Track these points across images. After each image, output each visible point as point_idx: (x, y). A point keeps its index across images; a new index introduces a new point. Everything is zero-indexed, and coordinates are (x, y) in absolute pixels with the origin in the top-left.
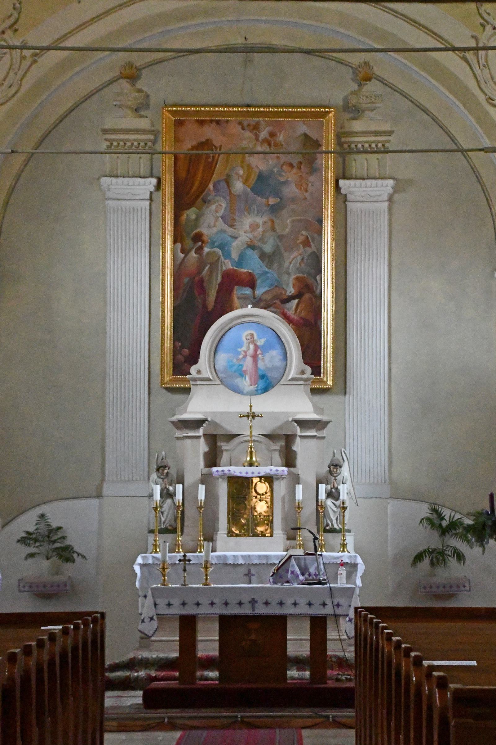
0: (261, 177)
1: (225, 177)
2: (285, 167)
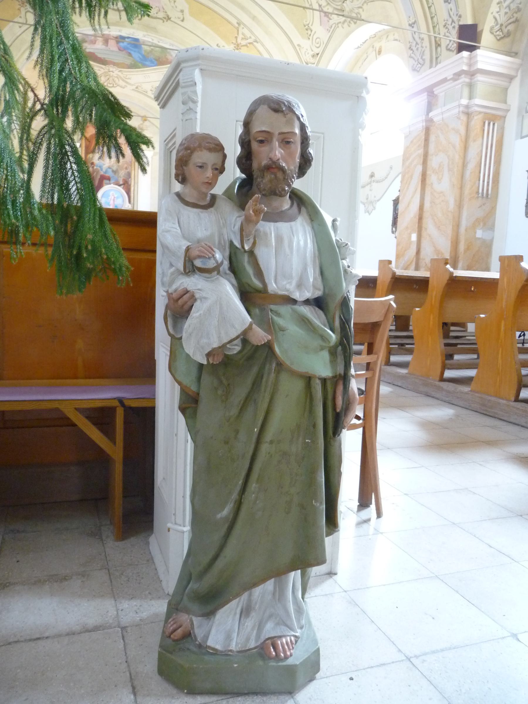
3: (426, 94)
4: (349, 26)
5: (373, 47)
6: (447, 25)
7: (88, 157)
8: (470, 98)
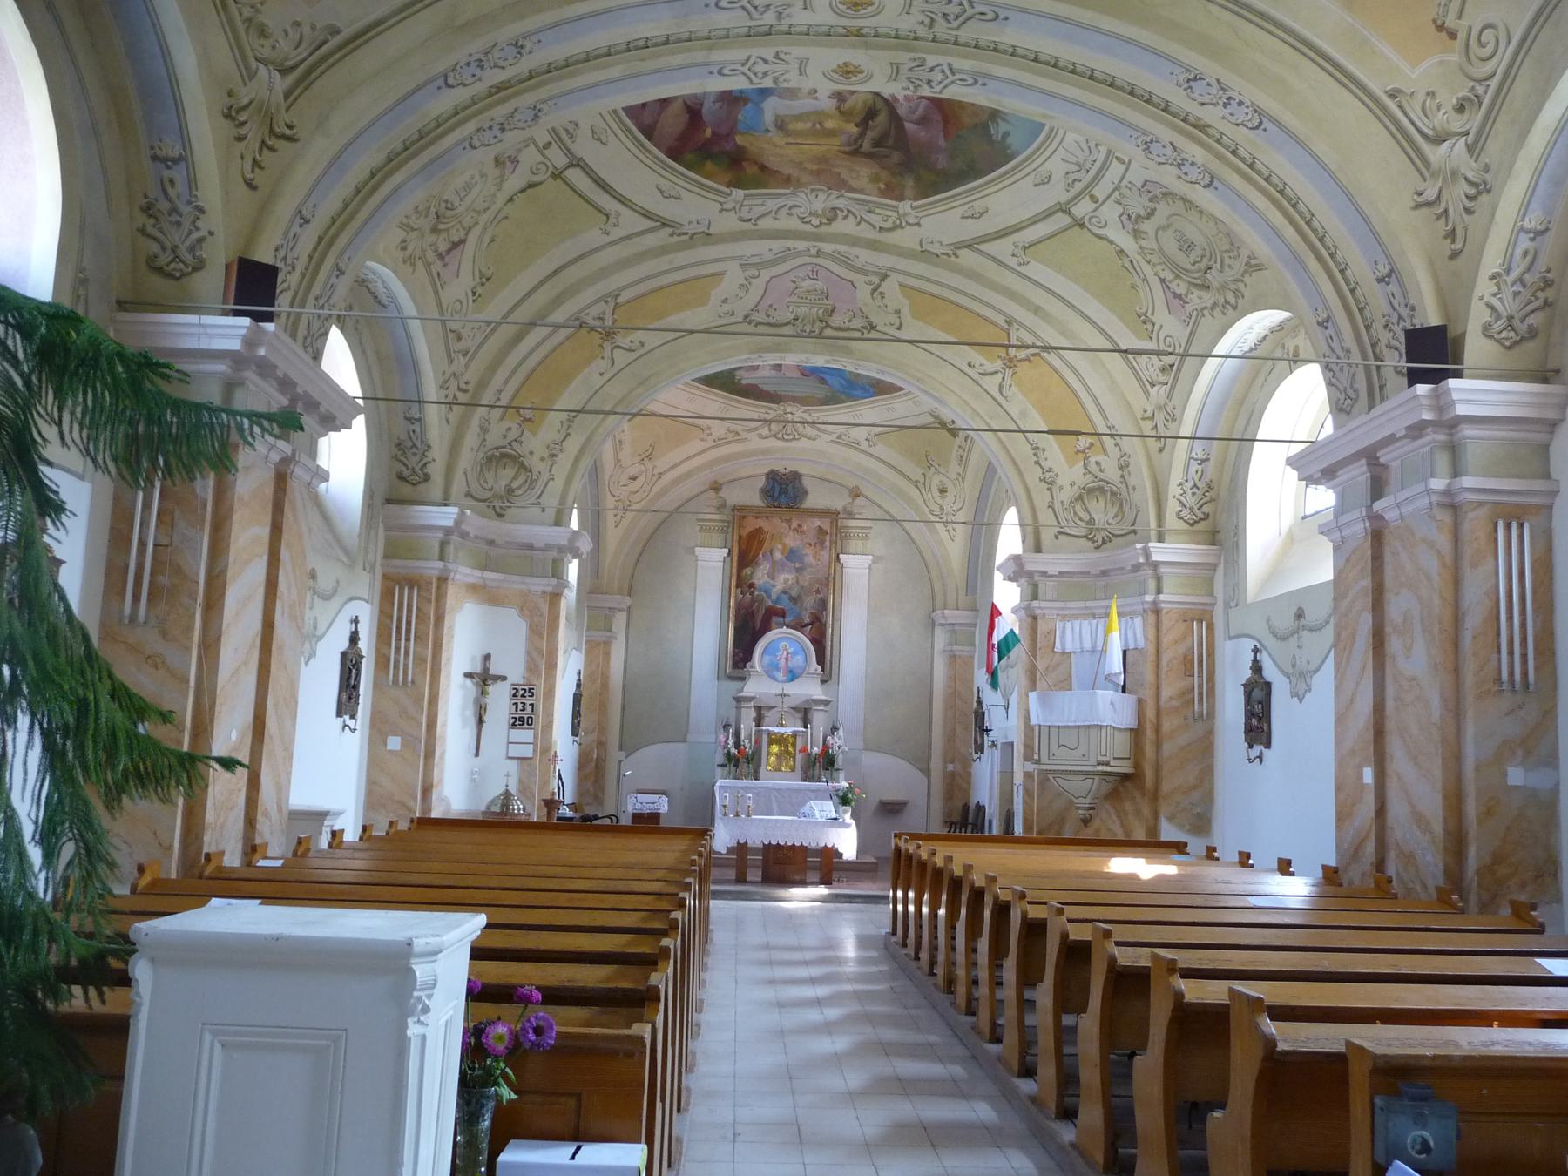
0: (792, 551)
3: (1364, 461)
4: (1224, 314)
5: (1283, 347)
6: (1390, 325)
8: (1456, 473)
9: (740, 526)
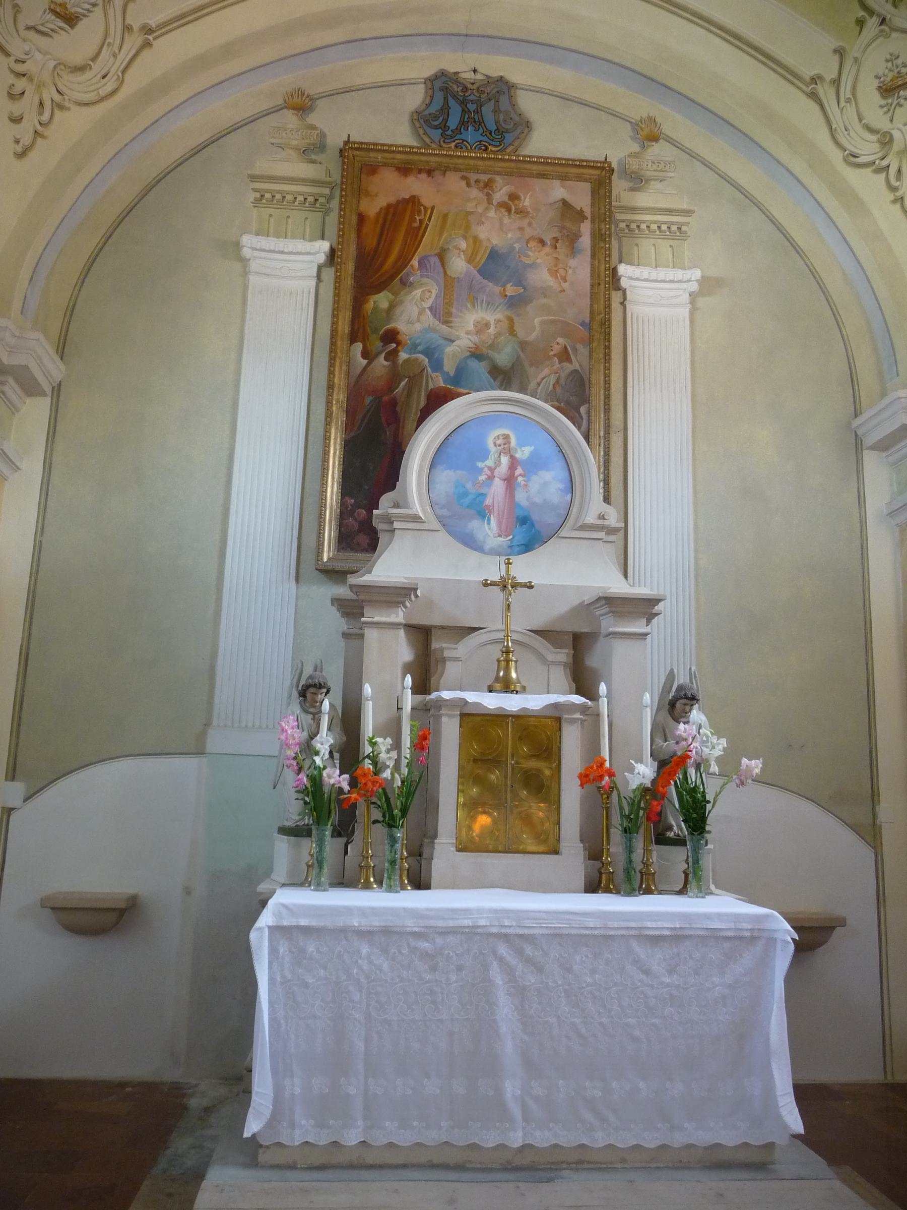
0: (494, 255)
1: (437, 251)
2: (532, 244)
7: (370, 305)
9: (360, 192)
